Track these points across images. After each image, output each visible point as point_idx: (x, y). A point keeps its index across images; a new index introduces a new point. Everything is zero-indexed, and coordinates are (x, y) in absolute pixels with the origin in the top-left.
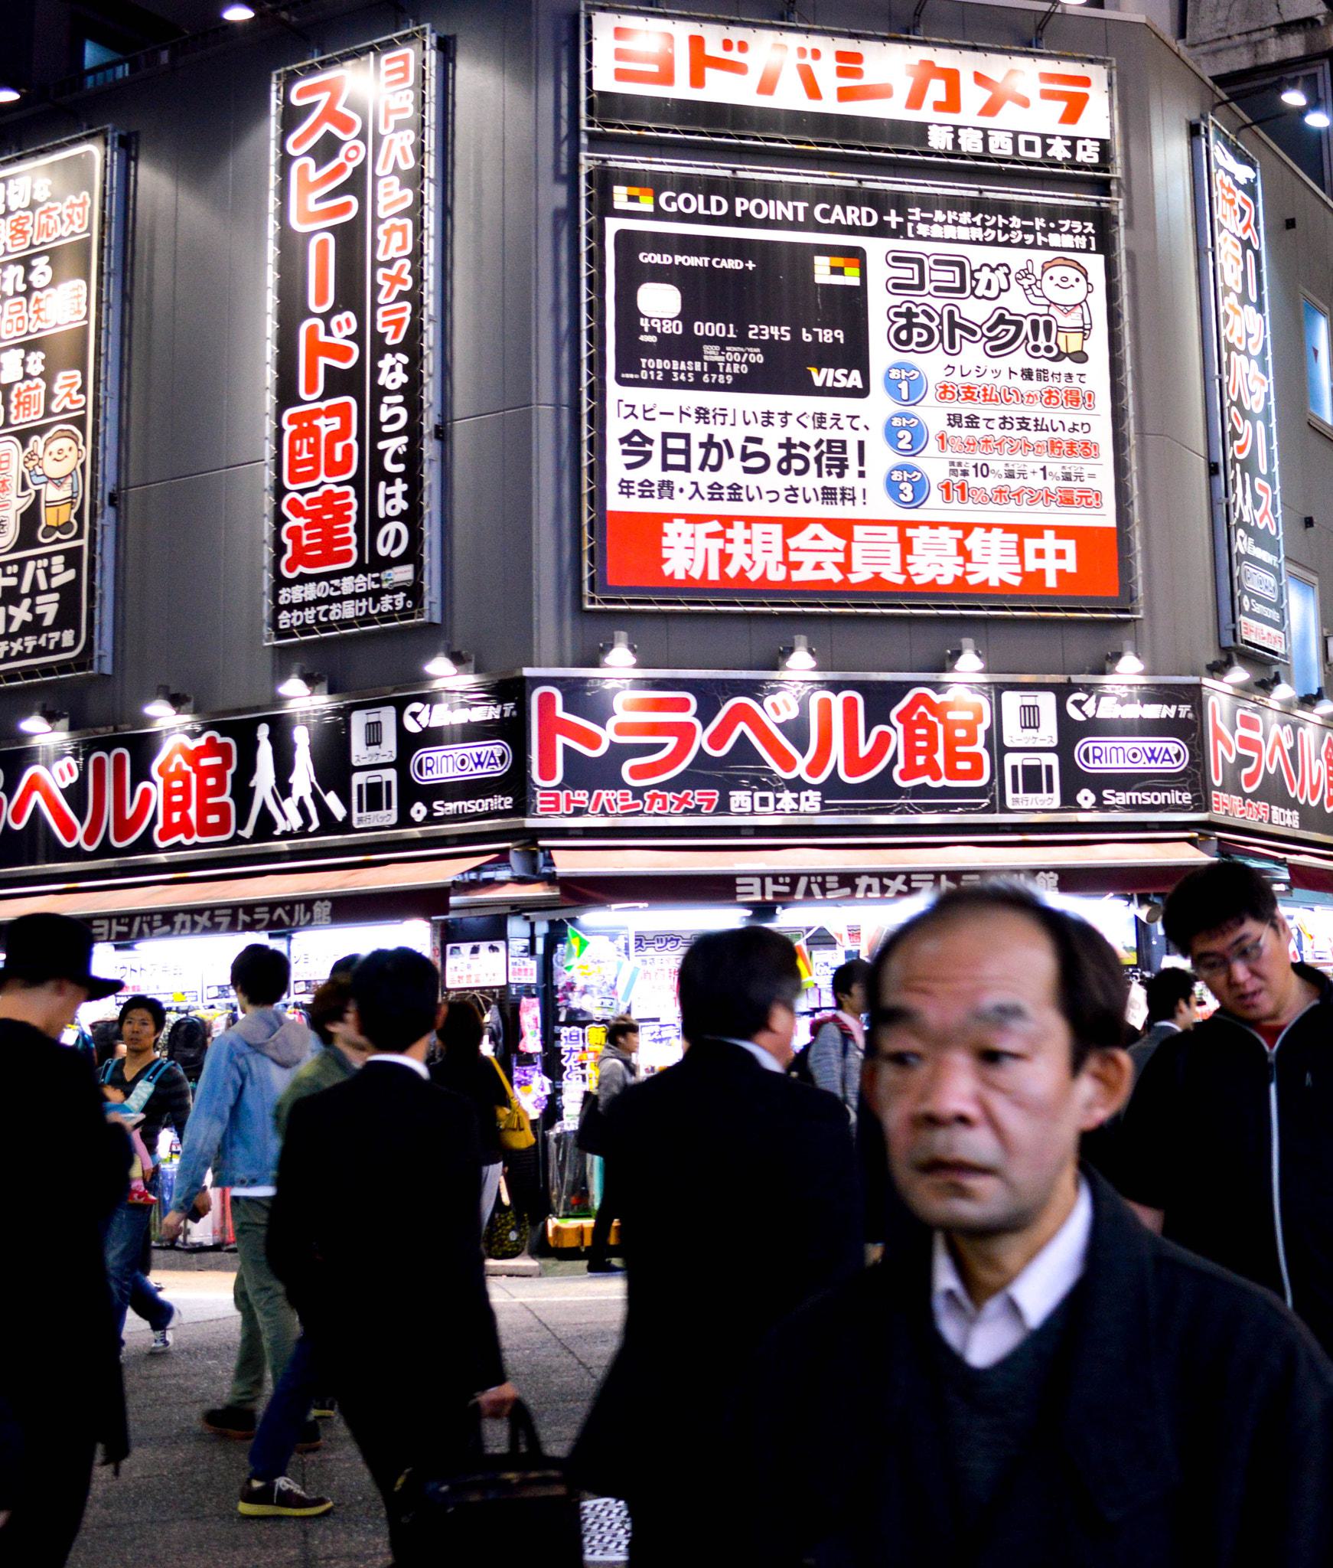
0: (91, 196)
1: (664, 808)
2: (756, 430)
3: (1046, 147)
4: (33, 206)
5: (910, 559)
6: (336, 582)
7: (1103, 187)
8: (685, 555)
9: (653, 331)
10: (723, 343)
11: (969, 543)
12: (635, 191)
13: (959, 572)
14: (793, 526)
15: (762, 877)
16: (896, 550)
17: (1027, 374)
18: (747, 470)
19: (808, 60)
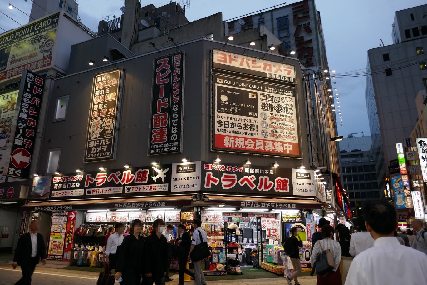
0: (118, 79)
1: (231, 170)
2: (240, 122)
3: (285, 79)
4: (107, 80)
5: (265, 146)
6: (162, 145)
7: (294, 86)
8: (228, 143)
9: (223, 103)
10: (234, 106)
11: (275, 144)
12: (220, 79)
13: (273, 149)
14: (246, 139)
15: (275, 203)
16: (263, 144)
17: (283, 116)
18: (238, 129)
19: (248, 61)
